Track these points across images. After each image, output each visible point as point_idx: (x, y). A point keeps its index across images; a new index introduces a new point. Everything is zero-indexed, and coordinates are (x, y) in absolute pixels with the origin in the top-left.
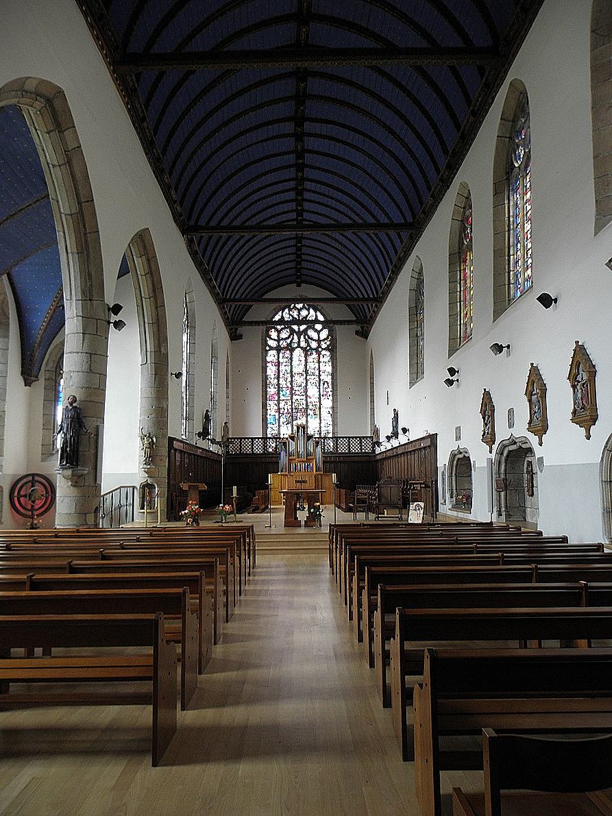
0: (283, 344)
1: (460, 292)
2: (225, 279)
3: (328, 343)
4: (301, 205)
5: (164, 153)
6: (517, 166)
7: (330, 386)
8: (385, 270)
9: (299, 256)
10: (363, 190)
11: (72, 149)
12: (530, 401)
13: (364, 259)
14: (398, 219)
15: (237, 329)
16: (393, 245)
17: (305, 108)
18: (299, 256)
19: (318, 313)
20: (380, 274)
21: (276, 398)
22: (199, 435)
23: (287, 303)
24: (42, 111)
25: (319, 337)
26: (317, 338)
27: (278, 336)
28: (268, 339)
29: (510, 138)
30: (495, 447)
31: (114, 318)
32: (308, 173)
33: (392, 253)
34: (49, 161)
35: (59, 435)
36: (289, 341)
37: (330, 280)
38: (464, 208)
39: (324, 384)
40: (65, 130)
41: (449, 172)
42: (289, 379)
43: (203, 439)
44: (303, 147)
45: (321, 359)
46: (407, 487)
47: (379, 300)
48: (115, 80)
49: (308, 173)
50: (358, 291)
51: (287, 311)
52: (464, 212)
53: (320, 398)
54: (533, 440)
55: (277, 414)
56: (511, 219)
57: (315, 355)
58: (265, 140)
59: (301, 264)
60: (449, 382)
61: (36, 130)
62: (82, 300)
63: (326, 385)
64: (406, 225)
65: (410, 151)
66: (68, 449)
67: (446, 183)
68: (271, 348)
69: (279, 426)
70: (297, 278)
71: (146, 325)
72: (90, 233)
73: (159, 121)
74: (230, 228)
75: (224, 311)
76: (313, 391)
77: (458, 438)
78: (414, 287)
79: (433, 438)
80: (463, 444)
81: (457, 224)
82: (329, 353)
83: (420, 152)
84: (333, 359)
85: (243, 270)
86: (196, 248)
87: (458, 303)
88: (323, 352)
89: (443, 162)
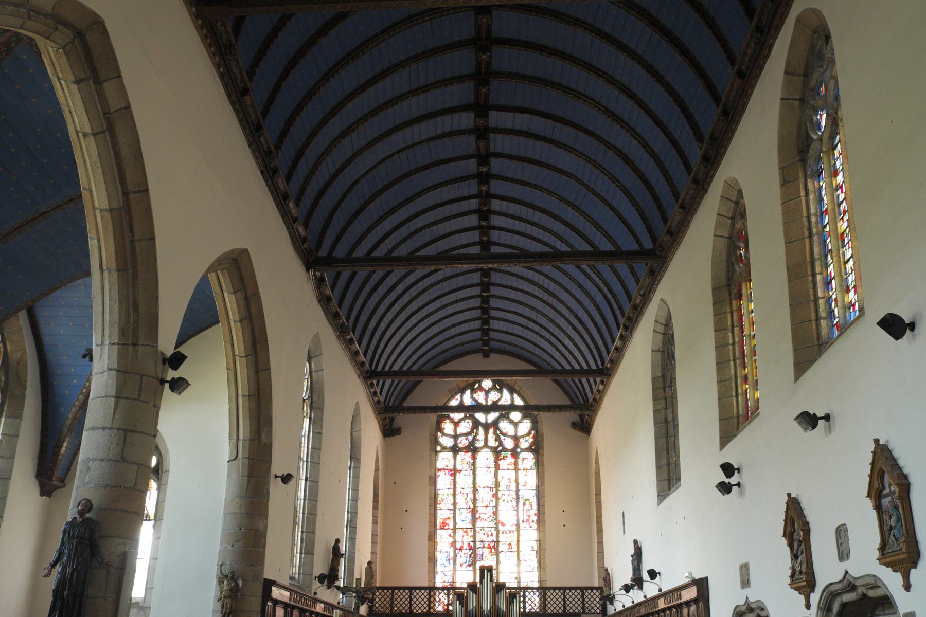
0: (463, 442)
1: (734, 344)
2: (374, 342)
4: (486, 234)
6: (815, 137)
8: (613, 326)
9: (485, 311)
10: (577, 209)
11: (115, 111)
12: (878, 508)
13: (581, 313)
14: (629, 244)
15: (393, 419)
16: (624, 286)
17: (489, 90)
18: (485, 311)
19: (515, 396)
20: (606, 334)
21: (451, 526)
22: (321, 579)
23: (472, 379)
25: (516, 431)
26: (453, 434)
27: (455, 431)
28: (439, 434)
29: (802, 100)
30: (815, 598)
31: (171, 374)
32: (496, 187)
33: (623, 298)
34: (79, 129)
36: (470, 438)
37: (526, 345)
38: (733, 218)
39: (524, 504)
40: (105, 81)
41: (706, 167)
42: (471, 496)
43: (329, 587)
44: (487, 148)
45: (520, 466)
47: (605, 372)
48: (199, 28)
49: (496, 187)
50: (570, 358)
51: (468, 392)
52: (733, 225)
53: (518, 525)
54: (891, 580)
56: (813, 219)
57: (510, 460)
58: (433, 139)
59: (488, 324)
60: (725, 488)
61: (59, 79)
62: (118, 344)
63: (528, 506)
64: (642, 254)
65: (645, 144)
66: (65, 593)
67: (701, 185)
68: (444, 449)
69: (454, 570)
70: (484, 345)
71: (240, 398)
72: (140, 240)
73: (271, 99)
75: (372, 390)
76: (507, 514)
77: (745, 583)
78: (659, 344)
79: (702, 585)
80: (754, 594)
81: (723, 243)
83: (659, 142)
86: (328, 292)
87: (732, 363)
88: (523, 455)
89: (695, 153)
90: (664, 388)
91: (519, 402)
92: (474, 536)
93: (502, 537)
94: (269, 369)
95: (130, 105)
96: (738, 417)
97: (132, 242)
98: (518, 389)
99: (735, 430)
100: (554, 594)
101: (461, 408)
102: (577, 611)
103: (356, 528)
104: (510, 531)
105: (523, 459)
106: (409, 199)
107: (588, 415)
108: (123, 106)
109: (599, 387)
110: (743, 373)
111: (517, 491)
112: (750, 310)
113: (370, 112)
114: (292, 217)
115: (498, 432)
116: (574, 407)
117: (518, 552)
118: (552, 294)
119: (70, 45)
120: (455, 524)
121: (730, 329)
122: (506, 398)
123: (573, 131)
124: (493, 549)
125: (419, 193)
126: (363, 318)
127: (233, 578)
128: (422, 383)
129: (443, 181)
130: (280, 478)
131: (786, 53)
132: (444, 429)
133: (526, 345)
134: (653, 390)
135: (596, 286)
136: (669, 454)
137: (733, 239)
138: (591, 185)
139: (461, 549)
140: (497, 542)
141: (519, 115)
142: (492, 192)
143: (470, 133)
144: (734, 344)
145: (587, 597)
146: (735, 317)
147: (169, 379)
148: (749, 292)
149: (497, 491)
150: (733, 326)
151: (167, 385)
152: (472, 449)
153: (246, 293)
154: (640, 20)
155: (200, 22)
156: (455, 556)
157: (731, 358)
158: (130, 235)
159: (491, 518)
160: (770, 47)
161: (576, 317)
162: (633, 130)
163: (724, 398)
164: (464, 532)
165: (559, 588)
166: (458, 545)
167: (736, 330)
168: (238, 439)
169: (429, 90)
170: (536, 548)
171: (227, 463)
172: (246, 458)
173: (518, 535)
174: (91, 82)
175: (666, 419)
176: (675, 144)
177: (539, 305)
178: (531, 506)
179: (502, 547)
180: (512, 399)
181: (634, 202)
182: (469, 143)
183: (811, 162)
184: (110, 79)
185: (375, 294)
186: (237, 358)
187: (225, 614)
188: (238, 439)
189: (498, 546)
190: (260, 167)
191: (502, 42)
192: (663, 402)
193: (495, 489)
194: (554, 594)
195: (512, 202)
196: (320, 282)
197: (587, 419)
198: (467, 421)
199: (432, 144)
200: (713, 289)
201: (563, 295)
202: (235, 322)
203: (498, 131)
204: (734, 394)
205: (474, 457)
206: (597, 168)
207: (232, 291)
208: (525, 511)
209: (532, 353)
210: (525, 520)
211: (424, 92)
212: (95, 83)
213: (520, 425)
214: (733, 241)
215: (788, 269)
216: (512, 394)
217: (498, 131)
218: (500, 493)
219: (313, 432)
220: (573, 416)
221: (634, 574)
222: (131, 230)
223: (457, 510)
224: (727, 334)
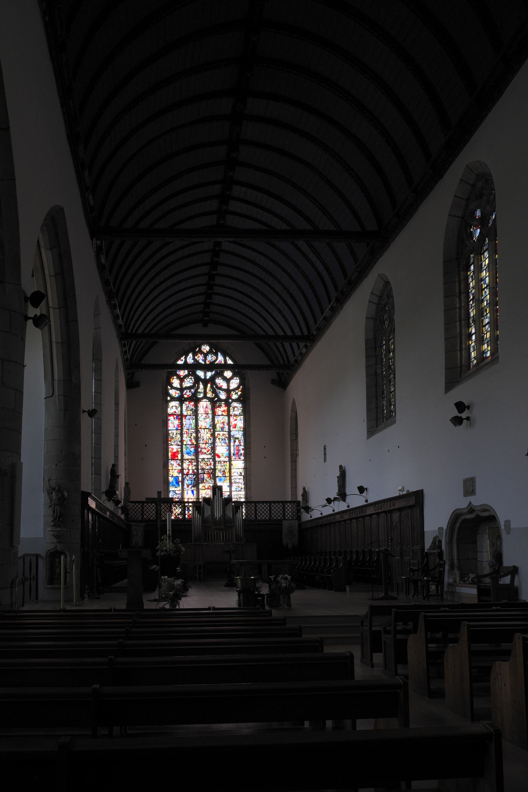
0: (187, 394)
1: (460, 308)
3: (239, 393)
7: (242, 444)
27: (181, 385)
31: (32, 312)
38: (468, 200)
42: (194, 435)
46: (306, 563)
51: (191, 355)
55: (180, 475)
57: (224, 408)
63: (237, 443)
71: (54, 345)
76: (221, 449)
79: (419, 495)
82: (241, 405)
84: (246, 412)
85: (147, 302)
87: (458, 323)
88: (235, 404)
91: (230, 362)
92: (197, 466)
93: (219, 467)
94: (77, 320)
96: (461, 367)
100: (263, 506)
101: (185, 366)
102: (279, 518)
103: (118, 457)
104: (224, 462)
105: (234, 408)
107: (287, 373)
110: (467, 332)
111: (229, 432)
112: (480, 278)
117: (230, 476)
118: (270, 274)
120: (182, 456)
124: (211, 475)
127: (60, 490)
130: (87, 413)
132: (173, 383)
136: (377, 400)
139: (188, 474)
140: (215, 469)
144: (460, 308)
145: (273, 510)
146: (462, 286)
148: (480, 263)
149: (214, 431)
150: (460, 293)
151: (30, 323)
152: (195, 399)
156: (183, 479)
157: (458, 320)
159: (210, 452)
164: (190, 462)
165: (266, 502)
166: (185, 472)
167: (463, 296)
168: (53, 380)
170: (243, 474)
171: (44, 400)
172: (61, 395)
173: (230, 465)
175: (376, 372)
178: (240, 443)
179: (218, 474)
180: (225, 360)
187: (56, 518)
188: (53, 380)
189: (215, 472)
193: (212, 430)
194: (263, 506)
196: (99, 250)
200: (444, 262)
202: (50, 276)
204: (459, 349)
205: (196, 406)
208: (235, 447)
210: (235, 453)
218: (216, 433)
219: (95, 379)
221: (339, 490)
223: (184, 446)
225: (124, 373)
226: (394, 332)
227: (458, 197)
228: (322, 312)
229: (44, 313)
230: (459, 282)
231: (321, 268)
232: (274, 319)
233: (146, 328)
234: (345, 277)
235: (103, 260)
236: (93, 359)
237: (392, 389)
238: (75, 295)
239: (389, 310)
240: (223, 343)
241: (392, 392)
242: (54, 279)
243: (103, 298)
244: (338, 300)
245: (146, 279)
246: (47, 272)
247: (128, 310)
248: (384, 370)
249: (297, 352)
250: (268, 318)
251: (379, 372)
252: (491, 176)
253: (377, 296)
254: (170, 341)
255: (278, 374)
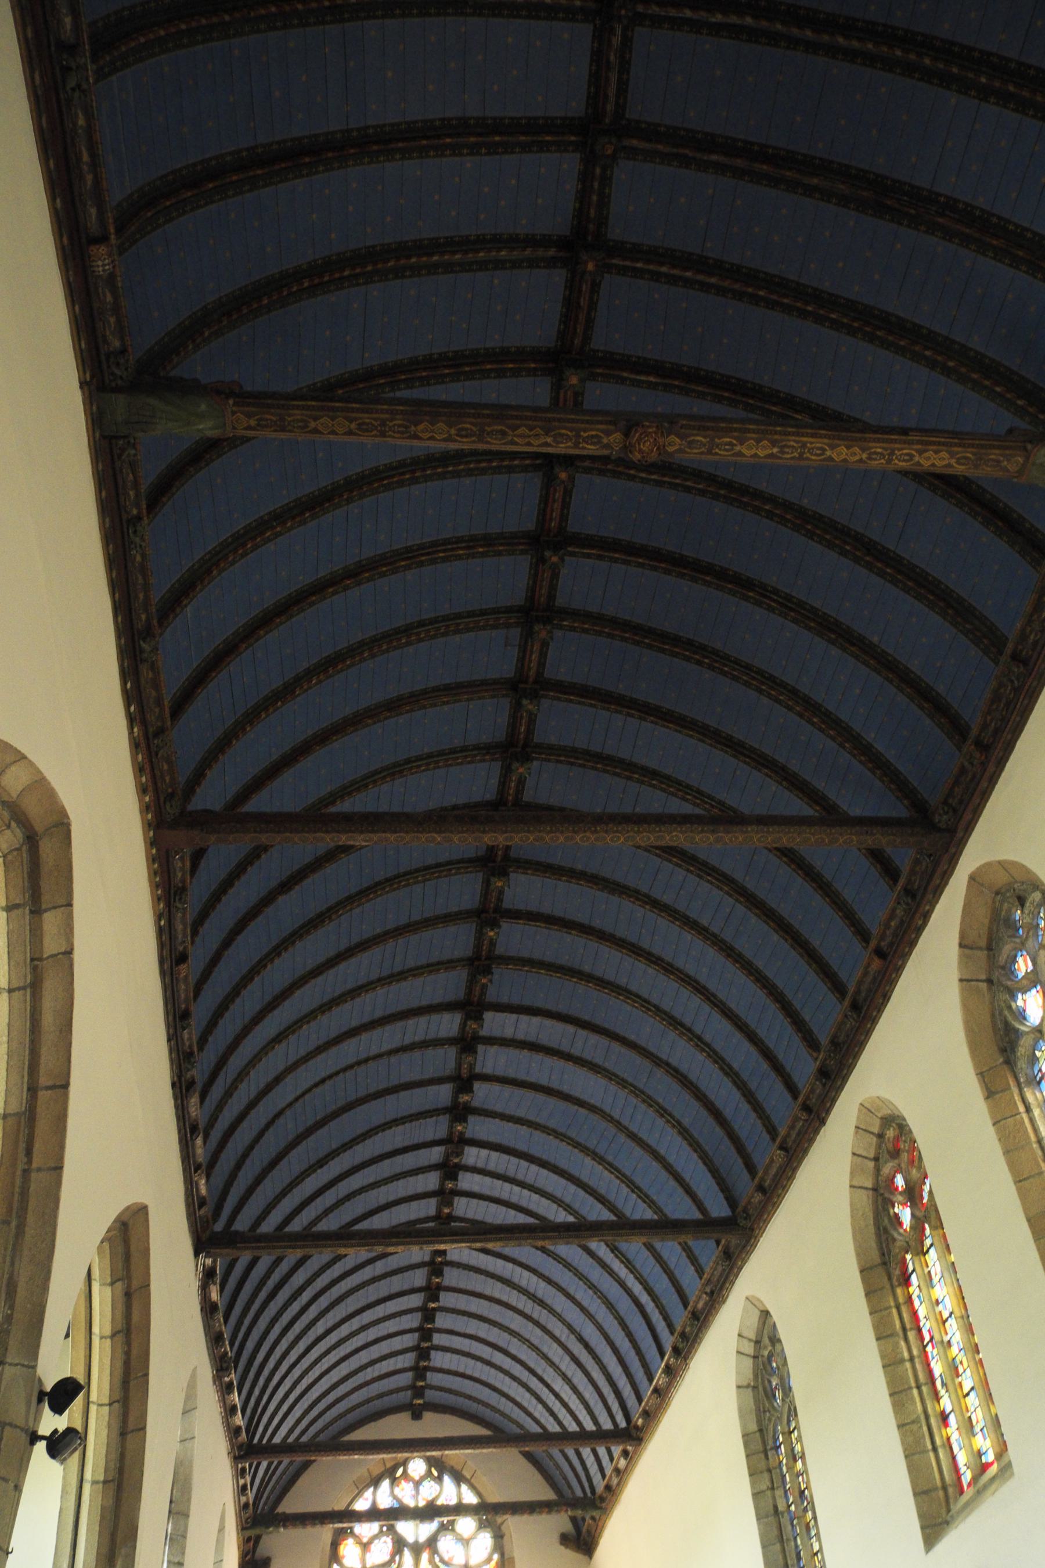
1: (912, 1359)
5: (203, 1041)
13: (590, 1332)
15: (258, 1539)
17: (491, 981)
19: (464, 1487)
24: (10, 857)
29: (990, 981)
31: (50, 1423)
33: (671, 1300)
35: (950, 1308)
37: (485, 1394)
38: (876, 1159)
41: (824, 1085)
48: (152, 860)
49: (477, 1127)
51: (386, 1484)
52: (878, 1170)
65: (716, 1057)
72: (39, 1170)
74: (310, 1238)
81: (865, 1199)
85: (297, 1372)
87: (915, 1392)
90: (765, 1452)
95: (72, 949)
97: (26, 1172)
98: (468, 1477)
99: (944, 1511)
101: (373, 1514)
106: (346, 1144)
107: (593, 1518)
108: (63, 950)
109: (618, 1463)
112: (934, 1300)
113: (321, 1006)
114: (194, 1161)
115: (437, 1559)
116: (562, 1501)
118: (541, 1303)
119: (15, 853)
121: (901, 1333)
122: (448, 1493)
123: (604, 1041)
125: (363, 1135)
126: (250, 1345)
128: (315, 1464)
129: (400, 1115)
131: (958, 922)
133: (485, 1394)
134: (747, 1456)
135: (620, 1284)
137: (882, 1191)
138: (625, 1122)
141: (524, 1018)
142: (468, 1135)
143: (451, 1044)
144: (912, 1359)
147: (45, 1430)
150: (904, 1329)
151: (41, 1447)
153: (129, 1286)
154: (718, 887)
155: (154, 851)
157: (913, 1384)
158: (25, 1160)
160: (926, 917)
161: (581, 1339)
162: (699, 1038)
163: (913, 1454)
167: (912, 1335)
169: (405, 979)
174: (27, 911)
175: (776, 1507)
176: (768, 1055)
177: (516, 1323)
181: (695, 1145)
182: (445, 1060)
183: (1022, 1064)
184: (55, 908)
185: (272, 1304)
186: (93, 1408)
190: (172, 1078)
191: (516, 915)
192: (766, 1475)
195: (496, 1150)
196: (208, 1275)
197: (589, 1525)
198: (384, 1538)
199: (393, 1059)
200: (861, 1271)
201: (560, 1302)
202: (101, 1338)
203: (491, 1041)
204: (930, 1447)
206: (637, 1096)
207: (109, 1280)
209: (494, 1409)
211: (398, 981)
212: (31, 912)
213: (473, 1544)
214: (882, 1195)
215: (1029, 1220)
216: (459, 1486)
217: (491, 1041)
220: (560, 1521)
222: (29, 1152)
224: (898, 1343)
225: (238, 1538)
226: (796, 1415)
227: (859, 1156)
228: (650, 1379)
229: (78, 1426)
230: (898, 1307)
231: (637, 1289)
232: (557, 1395)
233: (291, 1431)
234: (685, 1305)
235: (214, 1295)
236: (170, 1512)
237: (816, 1548)
238: (146, 1375)
239: (778, 1367)
240: (452, 1455)
241: (816, 1554)
242: (108, 1342)
243: (206, 1372)
244: (676, 1351)
245: (297, 1328)
246: (96, 1329)
247: (257, 1392)
248: (791, 1500)
249: (609, 1470)
250: (544, 1393)
251: (781, 1507)
252: (904, 1119)
253: (750, 1340)
254: (341, 1458)
255: (573, 1520)
